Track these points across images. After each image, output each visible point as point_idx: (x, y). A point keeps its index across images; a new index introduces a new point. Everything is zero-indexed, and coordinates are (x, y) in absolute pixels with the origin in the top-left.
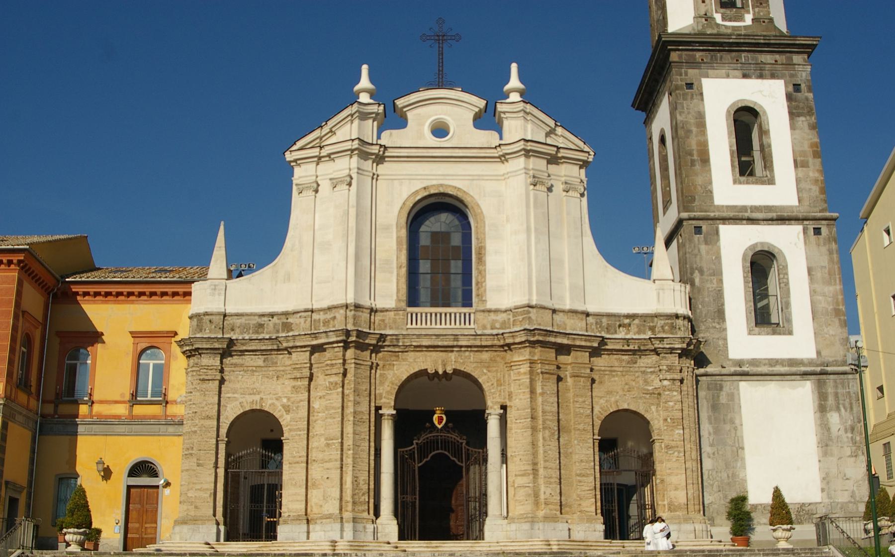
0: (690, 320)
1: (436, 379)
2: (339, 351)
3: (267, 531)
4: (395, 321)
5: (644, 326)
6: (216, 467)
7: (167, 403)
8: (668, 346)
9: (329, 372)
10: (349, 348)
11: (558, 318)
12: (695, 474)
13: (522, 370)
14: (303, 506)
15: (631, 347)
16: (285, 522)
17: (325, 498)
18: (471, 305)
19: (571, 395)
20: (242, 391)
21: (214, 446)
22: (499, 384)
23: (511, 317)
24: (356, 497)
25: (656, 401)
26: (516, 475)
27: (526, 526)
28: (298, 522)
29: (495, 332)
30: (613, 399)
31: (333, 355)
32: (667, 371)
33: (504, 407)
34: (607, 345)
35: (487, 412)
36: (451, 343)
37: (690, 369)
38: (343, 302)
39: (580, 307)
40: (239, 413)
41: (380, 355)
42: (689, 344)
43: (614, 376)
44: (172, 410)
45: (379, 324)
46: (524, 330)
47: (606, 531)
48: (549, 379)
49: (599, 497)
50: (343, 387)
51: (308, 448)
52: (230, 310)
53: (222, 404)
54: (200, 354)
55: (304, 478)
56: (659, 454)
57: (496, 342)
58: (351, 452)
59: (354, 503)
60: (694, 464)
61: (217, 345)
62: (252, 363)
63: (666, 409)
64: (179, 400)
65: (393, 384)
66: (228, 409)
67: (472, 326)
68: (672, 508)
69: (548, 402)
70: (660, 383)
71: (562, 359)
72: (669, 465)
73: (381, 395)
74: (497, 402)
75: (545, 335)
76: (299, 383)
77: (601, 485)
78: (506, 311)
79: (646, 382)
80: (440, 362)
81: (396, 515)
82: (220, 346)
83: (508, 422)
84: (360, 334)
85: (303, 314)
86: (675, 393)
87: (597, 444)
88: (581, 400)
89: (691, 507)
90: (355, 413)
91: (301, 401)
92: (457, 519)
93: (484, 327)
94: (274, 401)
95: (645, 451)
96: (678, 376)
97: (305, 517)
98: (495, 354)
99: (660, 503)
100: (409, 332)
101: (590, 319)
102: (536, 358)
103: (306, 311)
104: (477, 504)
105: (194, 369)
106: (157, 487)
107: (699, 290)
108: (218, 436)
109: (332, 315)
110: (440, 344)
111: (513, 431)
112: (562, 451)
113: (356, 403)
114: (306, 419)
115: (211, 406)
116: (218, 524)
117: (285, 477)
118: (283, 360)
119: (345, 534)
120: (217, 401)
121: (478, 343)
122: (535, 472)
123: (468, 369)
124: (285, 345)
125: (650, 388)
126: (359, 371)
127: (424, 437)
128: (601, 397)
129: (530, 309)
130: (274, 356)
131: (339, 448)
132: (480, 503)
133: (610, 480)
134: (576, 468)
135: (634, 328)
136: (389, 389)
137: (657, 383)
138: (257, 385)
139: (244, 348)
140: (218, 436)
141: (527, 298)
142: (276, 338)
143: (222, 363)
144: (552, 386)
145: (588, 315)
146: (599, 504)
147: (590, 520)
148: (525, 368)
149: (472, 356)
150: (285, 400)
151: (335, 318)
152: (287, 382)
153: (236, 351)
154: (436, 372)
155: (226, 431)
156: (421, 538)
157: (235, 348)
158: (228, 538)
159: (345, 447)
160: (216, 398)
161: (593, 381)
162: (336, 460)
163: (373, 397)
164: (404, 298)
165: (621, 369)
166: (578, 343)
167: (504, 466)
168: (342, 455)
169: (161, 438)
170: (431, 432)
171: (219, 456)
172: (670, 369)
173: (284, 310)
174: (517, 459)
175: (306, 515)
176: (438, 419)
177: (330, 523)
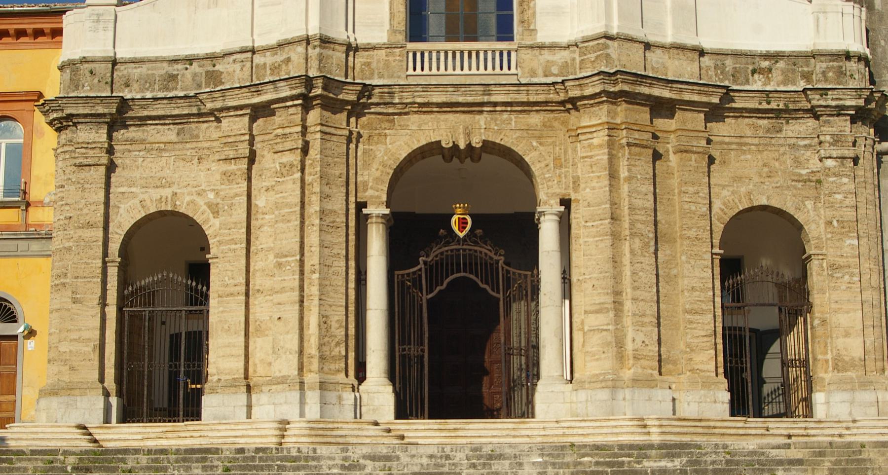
0: (867, 63)
1: (455, 160)
2: (296, 114)
3: (186, 404)
4: (387, 65)
5: (794, 71)
6: (103, 304)
7: (28, 205)
8: (834, 103)
9: (279, 147)
10: (312, 108)
11: (655, 57)
12: (877, 310)
13: (595, 141)
14: (241, 364)
15: (773, 105)
16: (213, 391)
17: (276, 351)
18: (511, 39)
19: (675, 182)
20: (143, 182)
21: (99, 271)
22: (558, 163)
23: (576, 56)
24: (325, 348)
25: (813, 192)
26: (586, 312)
27: (604, 395)
28: (233, 390)
29: (549, 80)
30: (743, 190)
31: (287, 119)
32: (831, 144)
33: (566, 203)
34: (733, 101)
35: (539, 209)
36: (479, 99)
37: (869, 142)
38: (302, 33)
39: (690, 41)
40: (139, 217)
41: (363, 120)
42: (868, 101)
43: (744, 152)
44: (37, 215)
45: (362, 71)
46: (598, 74)
47: (732, 402)
48: (640, 154)
49: (720, 347)
50: (303, 170)
51: (248, 271)
52: (123, 53)
53: (111, 204)
54: (75, 124)
55: (243, 319)
56: (817, 277)
57: (553, 97)
58: (317, 275)
59: (322, 358)
60: (876, 295)
61: (100, 110)
62: (159, 138)
63: (831, 206)
64: (47, 200)
65: (384, 166)
66: (121, 211)
67: (513, 70)
68: (839, 365)
69: (639, 193)
70: (819, 164)
71: (661, 123)
72: (835, 296)
73: (365, 184)
74: (554, 195)
75: (633, 83)
76: (232, 167)
77: (724, 328)
78: (568, 46)
79: (797, 162)
80: (461, 130)
81: (391, 376)
82: (106, 111)
83: (574, 226)
84: (329, 83)
85: (238, 56)
86: (845, 180)
87: (717, 262)
88: (691, 189)
89: (870, 364)
90: (322, 212)
91: (237, 195)
92: (491, 384)
93: (533, 73)
94: (195, 197)
95: (788, 274)
96: (850, 152)
97: (244, 382)
98: (552, 115)
99: (820, 357)
100: (411, 81)
101: (706, 61)
102: (618, 121)
103: (243, 51)
104: (523, 358)
105: (66, 148)
106: (15, 337)
107: (881, 17)
108: (105, 254)
109: (285, 56)
110: (461, 99)
111: (581, 241)
112: (661, 272)
113: (324, 197)
114: (245, 224)
115: (93, 207)
116: (107, 394)
117: (213, 319)
118: (207, 130)
119: (307, 409)
120: (102, 199)
121: (523, 98)
122: (618, 305)
123: (508, 140)
124: (210, 105)
125: (804, 172)
126: (328, 145)
127: (436, 253)
128: (724, 187)
129: (609, 42)
130: (193, 126)
131: (297, 269)
132: (527, 357)
133: (739, 321)
134: (685, 300)
135: (777, 76)
136: (378, 174)
137: (814, 164)
138: (167, 172)
139: (146, 113)
140: (105, 254)
141: (603, 23)
142: (195, 96)
143: (110, 137)
144: (644, 166)
145: (702, 53)
146: (721, 359)
147: (706, 385)
148: (600, 137)
149: (514, 120)
150: (211, 196)
151: (288, 60)
152: (214, 167)
153: (132, 118)
154: (455, 146)
155: (118, 246)
156: (435, 414)
157: (130, 114)
158: (127, 416)
159: (307, 268)
160: (102, 194)
161: (711, 160)
162: (292, 289)
163: (352, 187)
164: (402, 27)
165: (756, 141)
166: (687, 97)
167: (567, 302)
168: (302, 280)
169: (20, 260)
170: (447, 244)
171: (109, 286)
172: (837, 140)
173: (209, 51)
174: (589, 286)
175: (246, 377)
176: (459, 223)
177: (283, 390)
